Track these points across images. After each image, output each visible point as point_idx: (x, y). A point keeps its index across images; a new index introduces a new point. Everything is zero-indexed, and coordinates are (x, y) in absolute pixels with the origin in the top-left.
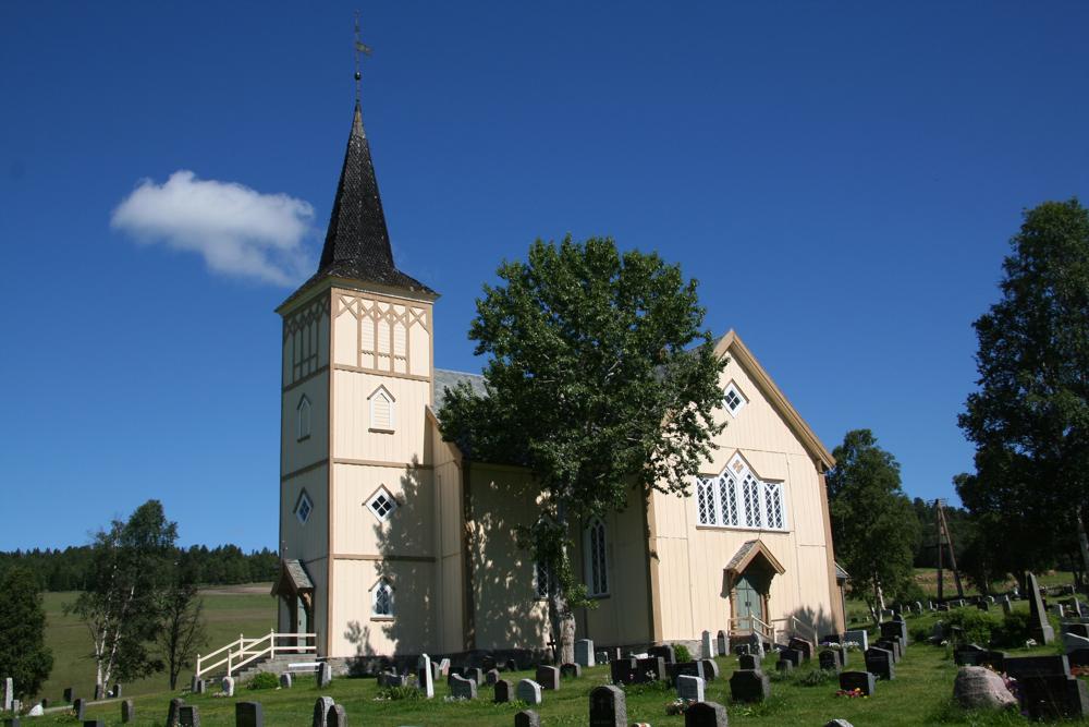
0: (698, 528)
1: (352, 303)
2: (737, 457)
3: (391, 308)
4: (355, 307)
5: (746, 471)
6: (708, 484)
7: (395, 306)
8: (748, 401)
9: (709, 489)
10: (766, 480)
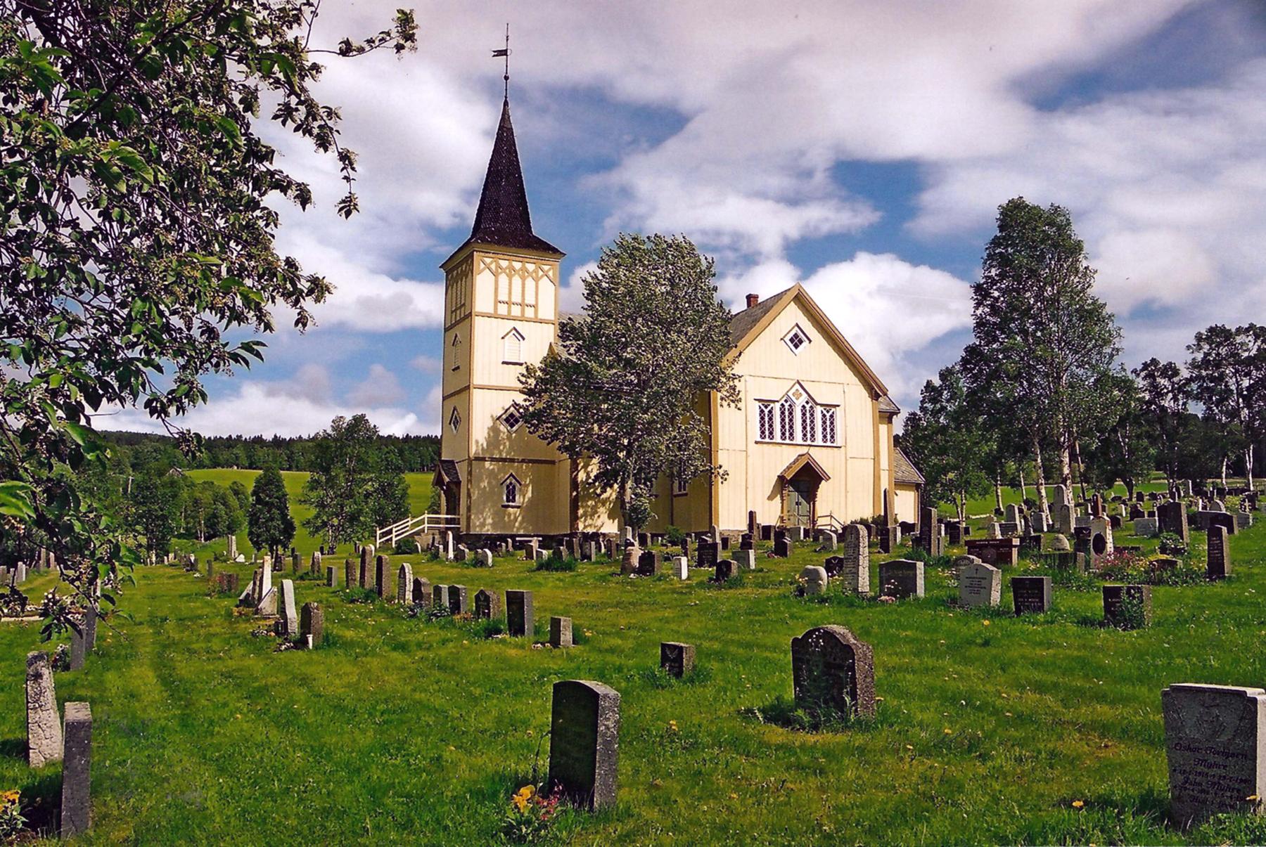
0: (756, 443)
1: (492, 263)
2: (797, 386)
3: (523, 265)
4: (493, 266)
5: (804, 397)
6: (769, 408)
7: (527, 265)
8: (810, 341)
9: (770, 412)
10: (822, 405)
